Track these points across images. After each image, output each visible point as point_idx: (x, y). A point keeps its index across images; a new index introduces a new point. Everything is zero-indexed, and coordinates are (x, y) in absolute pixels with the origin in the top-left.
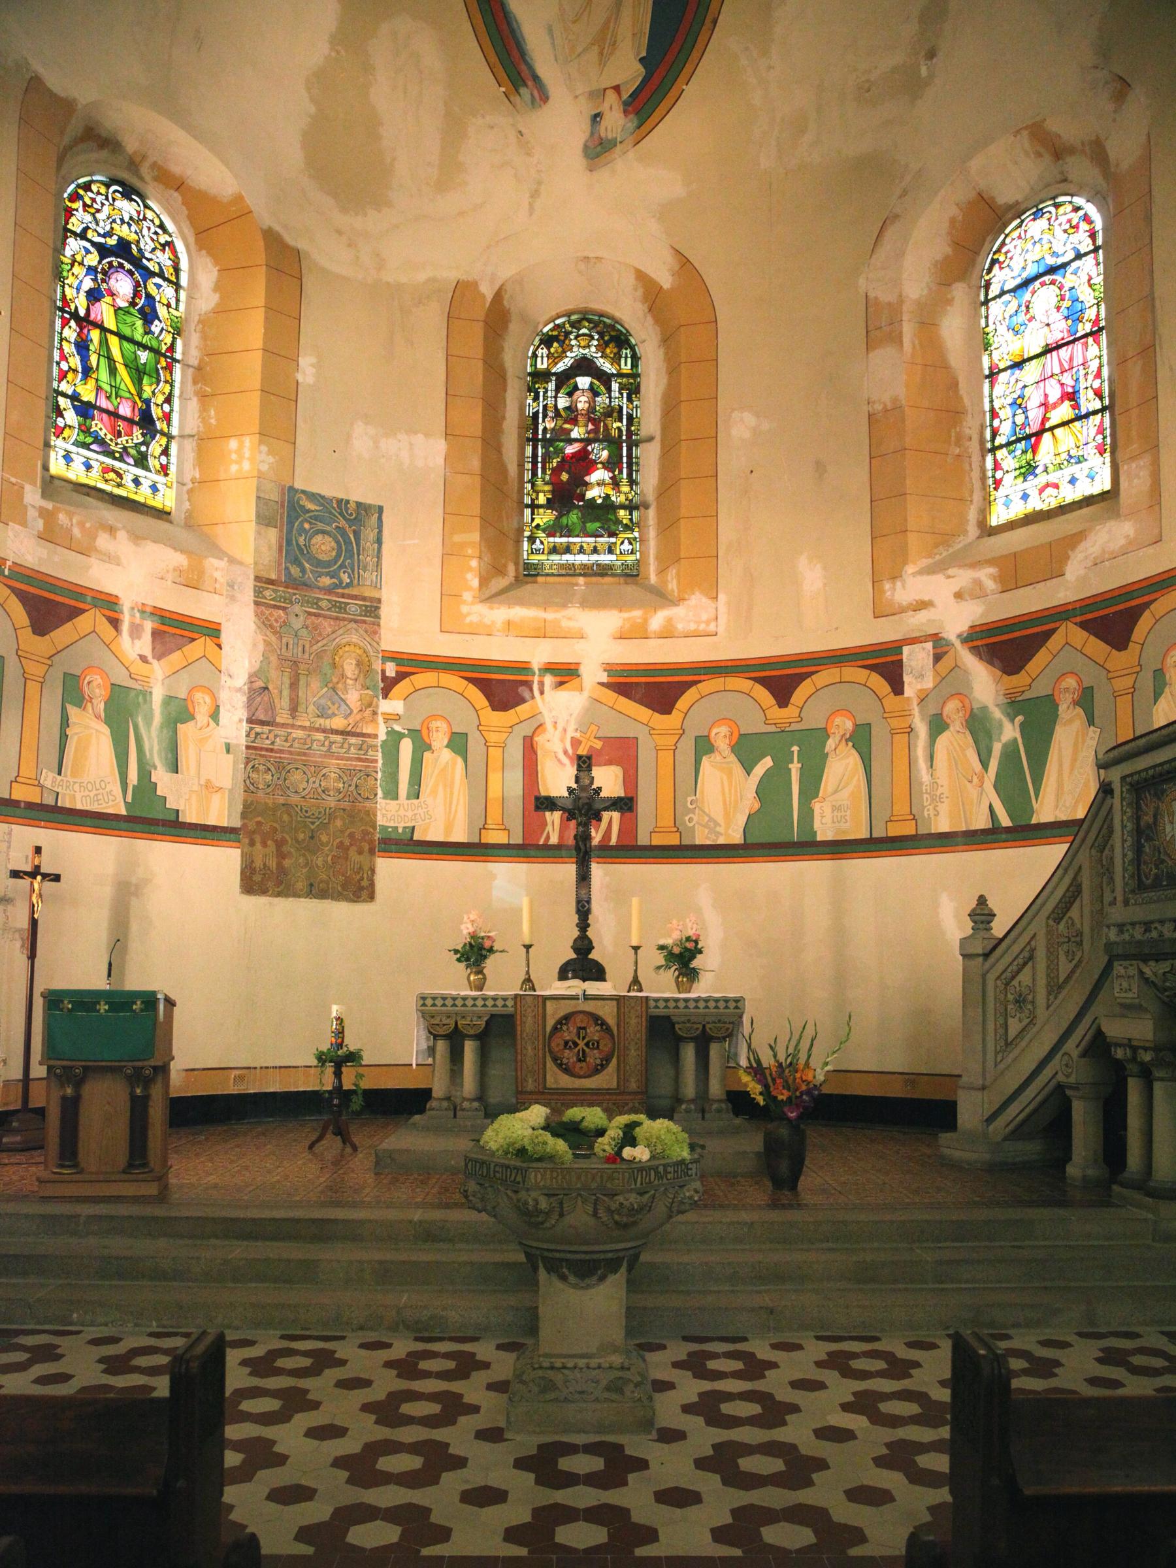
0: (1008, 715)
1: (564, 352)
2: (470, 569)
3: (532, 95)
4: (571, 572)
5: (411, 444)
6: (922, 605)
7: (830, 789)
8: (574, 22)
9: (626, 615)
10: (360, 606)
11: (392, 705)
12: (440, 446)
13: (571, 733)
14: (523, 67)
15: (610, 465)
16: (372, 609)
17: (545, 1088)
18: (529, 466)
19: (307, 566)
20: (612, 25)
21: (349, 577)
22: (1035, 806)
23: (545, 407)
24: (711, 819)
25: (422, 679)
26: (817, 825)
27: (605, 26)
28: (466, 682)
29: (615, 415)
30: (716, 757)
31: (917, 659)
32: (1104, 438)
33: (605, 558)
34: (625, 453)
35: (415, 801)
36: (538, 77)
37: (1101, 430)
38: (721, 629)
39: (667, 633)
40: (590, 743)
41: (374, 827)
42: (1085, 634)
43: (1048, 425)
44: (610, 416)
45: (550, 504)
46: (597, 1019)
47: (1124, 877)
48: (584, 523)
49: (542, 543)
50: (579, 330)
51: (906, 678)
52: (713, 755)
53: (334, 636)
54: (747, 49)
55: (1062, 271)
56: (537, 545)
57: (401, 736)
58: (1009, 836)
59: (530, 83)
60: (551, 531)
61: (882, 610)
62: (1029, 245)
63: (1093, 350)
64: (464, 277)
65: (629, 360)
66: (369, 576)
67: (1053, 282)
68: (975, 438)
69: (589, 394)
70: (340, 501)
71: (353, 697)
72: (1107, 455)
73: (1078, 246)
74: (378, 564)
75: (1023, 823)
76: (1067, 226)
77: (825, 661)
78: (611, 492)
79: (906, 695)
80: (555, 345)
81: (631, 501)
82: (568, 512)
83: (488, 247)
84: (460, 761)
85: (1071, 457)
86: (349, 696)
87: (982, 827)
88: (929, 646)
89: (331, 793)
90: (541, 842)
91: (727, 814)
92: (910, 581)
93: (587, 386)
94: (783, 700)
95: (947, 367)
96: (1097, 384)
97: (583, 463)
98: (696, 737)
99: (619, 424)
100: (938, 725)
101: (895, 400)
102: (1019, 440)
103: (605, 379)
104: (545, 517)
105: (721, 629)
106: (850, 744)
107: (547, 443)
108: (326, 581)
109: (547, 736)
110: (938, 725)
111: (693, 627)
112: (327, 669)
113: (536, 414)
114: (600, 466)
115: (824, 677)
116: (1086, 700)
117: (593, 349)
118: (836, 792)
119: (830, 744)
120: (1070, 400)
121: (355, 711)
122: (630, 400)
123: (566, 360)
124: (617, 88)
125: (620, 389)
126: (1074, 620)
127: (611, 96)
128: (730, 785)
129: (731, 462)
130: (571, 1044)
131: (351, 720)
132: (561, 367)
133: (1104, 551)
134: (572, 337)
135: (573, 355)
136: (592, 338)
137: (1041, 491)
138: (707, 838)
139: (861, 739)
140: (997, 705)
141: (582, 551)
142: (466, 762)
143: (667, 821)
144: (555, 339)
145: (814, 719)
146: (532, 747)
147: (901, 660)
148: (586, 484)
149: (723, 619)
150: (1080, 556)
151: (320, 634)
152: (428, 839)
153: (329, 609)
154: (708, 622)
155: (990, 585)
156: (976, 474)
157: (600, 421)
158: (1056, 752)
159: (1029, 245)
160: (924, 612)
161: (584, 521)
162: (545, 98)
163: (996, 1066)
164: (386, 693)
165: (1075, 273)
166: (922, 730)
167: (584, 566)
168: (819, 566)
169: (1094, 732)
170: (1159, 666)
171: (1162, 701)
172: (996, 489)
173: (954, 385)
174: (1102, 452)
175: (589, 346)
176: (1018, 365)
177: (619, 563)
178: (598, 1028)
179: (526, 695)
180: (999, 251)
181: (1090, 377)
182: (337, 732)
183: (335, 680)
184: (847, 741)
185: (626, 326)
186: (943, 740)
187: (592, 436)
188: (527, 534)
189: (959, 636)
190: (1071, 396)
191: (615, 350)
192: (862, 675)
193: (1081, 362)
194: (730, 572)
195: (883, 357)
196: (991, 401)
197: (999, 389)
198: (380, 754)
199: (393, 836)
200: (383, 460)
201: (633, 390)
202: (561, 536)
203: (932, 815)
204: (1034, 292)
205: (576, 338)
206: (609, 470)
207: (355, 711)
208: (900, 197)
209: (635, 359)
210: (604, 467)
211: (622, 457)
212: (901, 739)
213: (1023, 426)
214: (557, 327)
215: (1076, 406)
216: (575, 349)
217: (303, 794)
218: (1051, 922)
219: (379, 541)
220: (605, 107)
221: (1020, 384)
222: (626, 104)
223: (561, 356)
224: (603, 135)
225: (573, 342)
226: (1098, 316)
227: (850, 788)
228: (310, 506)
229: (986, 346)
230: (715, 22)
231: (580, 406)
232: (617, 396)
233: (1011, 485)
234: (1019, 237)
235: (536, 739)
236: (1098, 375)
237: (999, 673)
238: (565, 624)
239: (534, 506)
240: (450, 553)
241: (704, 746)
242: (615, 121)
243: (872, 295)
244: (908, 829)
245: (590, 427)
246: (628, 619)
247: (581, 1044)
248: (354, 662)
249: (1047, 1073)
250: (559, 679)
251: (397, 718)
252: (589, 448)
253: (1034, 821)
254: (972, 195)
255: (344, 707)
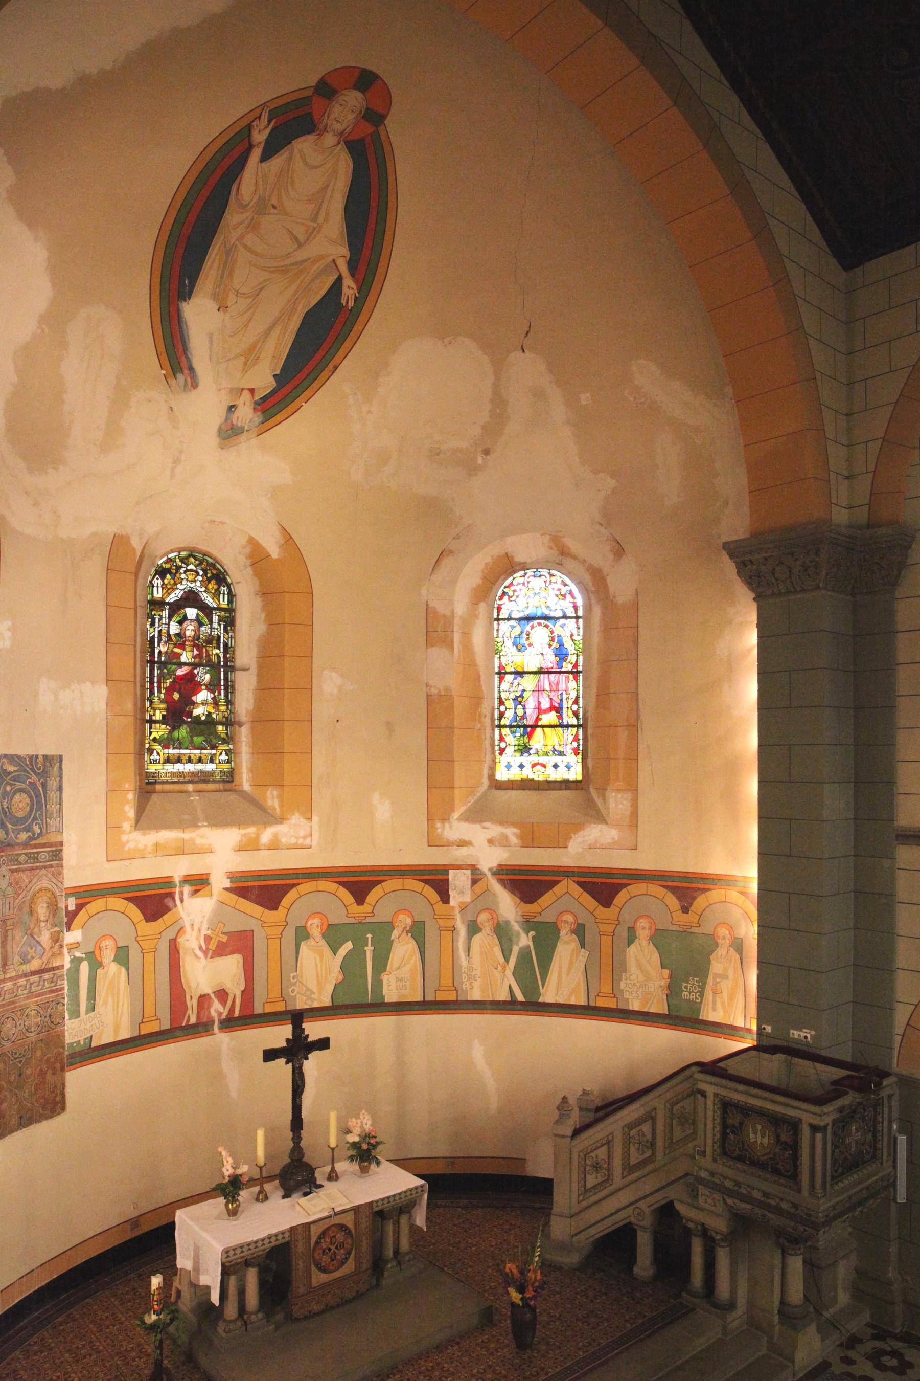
0: (524, 929)
1: (175, 584)
2: (128, 802)
3: (186, 380)
4: (182, 779)
5: (81, 693)
6: (463, 843)
7: (396, 965)
8: (230, 336)
9: (243, 831)
10: (48, 852)
11: (73, 936)
12: (102, 691)
13: (204, 932)
14: (184, 359)
15: (212, 687)
16: (57, 853)
17: (311, 1288)
18: (148, 685)
19: (10, 826)
20: (259, 346)
21: (40, 828)
22: (542, 991)
23: (160, 632)
24: (308, 989)
25: (95, 906)
26: (385, 992)
27: (252, 348)
28: (126, 902)
29: (214, 642)
30: (311, 942)
31: (459, 880)
32: (579, 745)
33: (209, 767)
34: (222, 678)
35: (92, 1014)
36: (193, 369)
37: (576, 739)
38: (314, 843)
39: (274, 846)
40: (218, 938)
41: (64, 1047)
42: (581, 890)
43: (540, 723)
44: (211, 643)
45: (164, 720)
46: (342, 1227)
47: (713, 1146)
48: (192, 737)
49: (158, 754)
50: (188, 565)
51: (451, 892)
52: (309, 941)
53: (30, 885)
54: (355, 394)
55: (553, 621)
56: (155, 756)
57: (80, 960)
58: (522, 1007)
59: (186, 372)
60: (166, 743)
61: (433, 841)
62: (531, 593)
63: (572, 684)
64: (118, 532)
65: (226, 596)
66: (53, 823)
67: (546, 626)
68: (489, 715)
69: (196, 624)
70: (31, 757)
71: (45, 938)
72: (580, 756)
73: (565, 610)
74: (60, 810)
75: (533, 1000)
76: (558, 593)
77: (392, 873)
78: (212, 711)
79: (451, 904)
80: (168, 576)
81: (227, 718)
82: (179, 727)
83: (138, 503)
84: (123, 970)
85: (555, 750)
86: (43, 937)
87: (504, 999)
88: (468, 872)
89: (33, 1029)
90: (184, 1024)
91: (319, 984)
92: (455, 824)
93: (194, 617)
94: (360, 900)
95: (475, 665)
96: (575, 708)
97: (189, 685)
98: (297, 928)
99: (217, 651)
100: (474, 929)
101: (447, 689)
102: (519, 726)
103: (207, 610)
104: (160, 731)
105: (314, 843)
106: (410, 935)
107: (162, 665)
108: (23, 836)
109: (187, 936)
110: (474, 929)
111: (293, 841)
112: (26, 917)
113: (153, 638)
114: (203, 687)
115: (391, 884)
116: (579, 931)
117: (198, 584)
118: (398, 968)
119: (395, 934)
120: (557, 712)
121: (47, 950)
122: (226, 630)
123: (177, 592)
124: (252, 391)
125: (219, 621)
126: (573, 878)
127: (246, 394)
128: (321, 961)
129: (322, 712)
130: (327, 1251)
131: (45, 958)
132: (173, 597)
133: (596, 841)
134: (182, 571)
135: (182, 587)
136: (198, 574)
137: (533, 766)
138: (306, 1004)
139: (417, 932)
140: (517, 922)
141: (190, 760)
142: (128, 969)
143: (276, 993)
144: (168, 571)
145: (383, 914)
146: (176, 946)
147: (448, 879)
148: (194, 703)
149: (316, 836)
150: (580, 840)
151: (20, 887)
152: (102, 1043)
153: (26, 863)
154: (304, 838)
155: (514, 840)
156: (487, 742)
157: (203, 646)
158: (558, 959)
159: (531, 593)
160: (465, 848)
161: (192, 733)
162: (195, 385)
163: (579, 1203)
164: (69, 927)
165: (562, 626)
166: (462, 930)
167: (191, 773)
168: (387, 802)
169: (585, 953)
170: (632, 925)
171: (633, 947)
172: (501, 754)
173: (478, 678)
174: (576, 754)
175: (195, 581)
176: (520, 674)
177: (218, 771)
178: (343, 1233)
179: (170, 904)
180: (508, 587)
181: (571, 702)
182: (34, 973)
183: (32, 926)
184: (407, 932)
185: (225, 567)
186: (477, 939)
187: (197, 660)
188: (147, 746)
189: (490, 870)
190: (558, 710)
191: (216, 587)
192: (419, 886)
193: (564, 688)
194: (321, 799)
195: (437, 654)
196: (500, 692)
197: (505, 686)
198: (66, 982)
199: (77, 1049)
200: (62, 711)
201: (229, 622)
202: (174, 748)
203: (468, 989)
204: (532, 627)
205: (185, 572)
206: (212, 692)
207: (47, 950)
208: (454, 538)
209: (231, 596)
210: (208, 689)
211: (220, 680)
212: (447, 936)
213: (523, 718)
214: (169, 560)
215: (560, 717)
216: (184, 582)
217: (13, 1039)
218: (626, 1129)
219: (60, 789)
220: (240, 402)
221: (521, 688)
222: (256, 403)
223: (173, 588)
224: (235, 422)
225: (183, 576)
226: (577, 662)
227: (408, 967)
228: (11, 768)
229: (497, 651)
230: (336, 368)
231: (188, 633)
232: (218, 629)
233: (510, 756)
234: (524, 584)
235: (179, 940)
236: (576, 702)
237: (519, 901)
238: (198, 841)
239: (152, 722)
240: (113, 789)
241: (302, 934)
242: (246, 414)
243: (431, 604)
244: (452, 997)
245: (196, 652)
246: (245, 835)
247: (333, 1248)
248: (45, 905)
249: (622, 1215)
250: (194, 888)
251: (77, 945)
252: (195, 671)
253: (541, 1000)
254: (503, 552)
255: (39, 948)
